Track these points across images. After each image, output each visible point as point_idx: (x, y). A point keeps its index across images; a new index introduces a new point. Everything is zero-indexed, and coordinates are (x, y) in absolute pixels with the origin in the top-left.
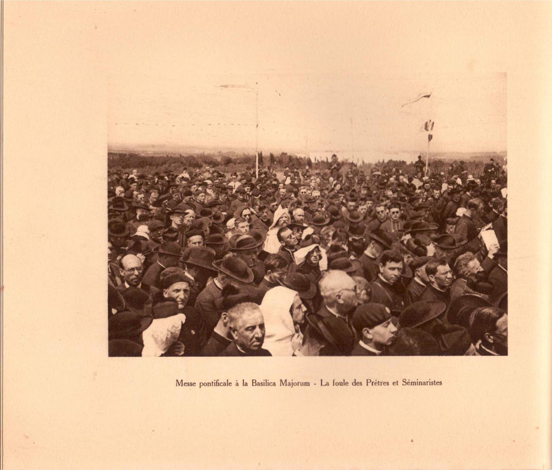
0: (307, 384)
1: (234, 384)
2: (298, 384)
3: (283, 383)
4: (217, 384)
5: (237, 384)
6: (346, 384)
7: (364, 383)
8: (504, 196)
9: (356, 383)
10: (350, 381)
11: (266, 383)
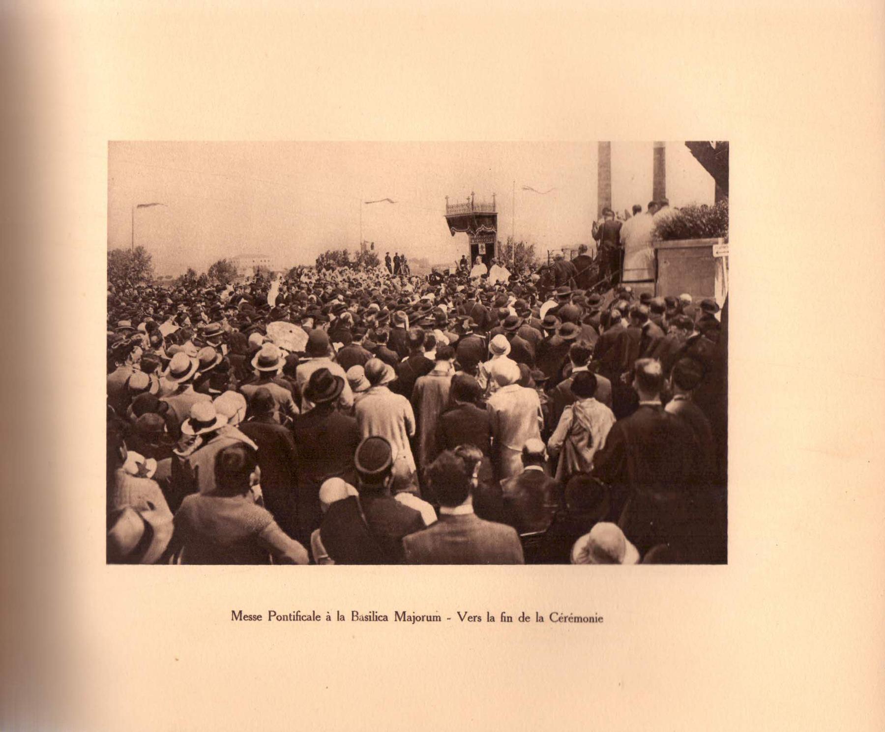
0: (438, 619)
1: (323, 618)
2: (422, 619)
3: (401, 616)
4: (298, 617)
5: (329, 618)
6: (317, 618)
7: (265, 616)
8: (684, 344)
9: (524, 618)
10: (515, 616)
11: (373, 617)
